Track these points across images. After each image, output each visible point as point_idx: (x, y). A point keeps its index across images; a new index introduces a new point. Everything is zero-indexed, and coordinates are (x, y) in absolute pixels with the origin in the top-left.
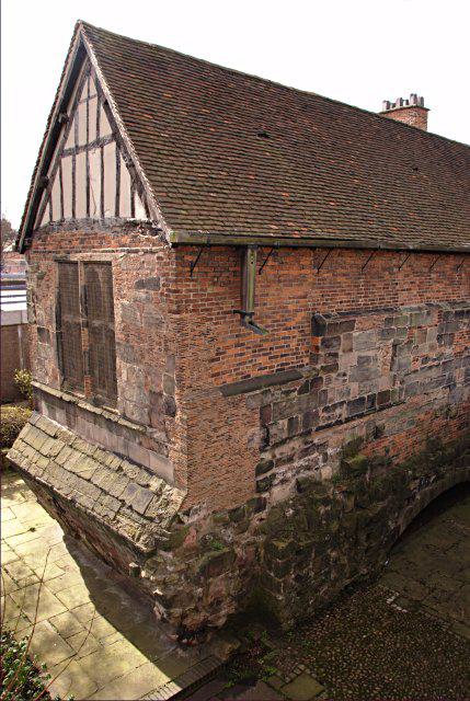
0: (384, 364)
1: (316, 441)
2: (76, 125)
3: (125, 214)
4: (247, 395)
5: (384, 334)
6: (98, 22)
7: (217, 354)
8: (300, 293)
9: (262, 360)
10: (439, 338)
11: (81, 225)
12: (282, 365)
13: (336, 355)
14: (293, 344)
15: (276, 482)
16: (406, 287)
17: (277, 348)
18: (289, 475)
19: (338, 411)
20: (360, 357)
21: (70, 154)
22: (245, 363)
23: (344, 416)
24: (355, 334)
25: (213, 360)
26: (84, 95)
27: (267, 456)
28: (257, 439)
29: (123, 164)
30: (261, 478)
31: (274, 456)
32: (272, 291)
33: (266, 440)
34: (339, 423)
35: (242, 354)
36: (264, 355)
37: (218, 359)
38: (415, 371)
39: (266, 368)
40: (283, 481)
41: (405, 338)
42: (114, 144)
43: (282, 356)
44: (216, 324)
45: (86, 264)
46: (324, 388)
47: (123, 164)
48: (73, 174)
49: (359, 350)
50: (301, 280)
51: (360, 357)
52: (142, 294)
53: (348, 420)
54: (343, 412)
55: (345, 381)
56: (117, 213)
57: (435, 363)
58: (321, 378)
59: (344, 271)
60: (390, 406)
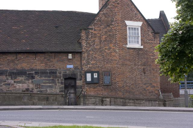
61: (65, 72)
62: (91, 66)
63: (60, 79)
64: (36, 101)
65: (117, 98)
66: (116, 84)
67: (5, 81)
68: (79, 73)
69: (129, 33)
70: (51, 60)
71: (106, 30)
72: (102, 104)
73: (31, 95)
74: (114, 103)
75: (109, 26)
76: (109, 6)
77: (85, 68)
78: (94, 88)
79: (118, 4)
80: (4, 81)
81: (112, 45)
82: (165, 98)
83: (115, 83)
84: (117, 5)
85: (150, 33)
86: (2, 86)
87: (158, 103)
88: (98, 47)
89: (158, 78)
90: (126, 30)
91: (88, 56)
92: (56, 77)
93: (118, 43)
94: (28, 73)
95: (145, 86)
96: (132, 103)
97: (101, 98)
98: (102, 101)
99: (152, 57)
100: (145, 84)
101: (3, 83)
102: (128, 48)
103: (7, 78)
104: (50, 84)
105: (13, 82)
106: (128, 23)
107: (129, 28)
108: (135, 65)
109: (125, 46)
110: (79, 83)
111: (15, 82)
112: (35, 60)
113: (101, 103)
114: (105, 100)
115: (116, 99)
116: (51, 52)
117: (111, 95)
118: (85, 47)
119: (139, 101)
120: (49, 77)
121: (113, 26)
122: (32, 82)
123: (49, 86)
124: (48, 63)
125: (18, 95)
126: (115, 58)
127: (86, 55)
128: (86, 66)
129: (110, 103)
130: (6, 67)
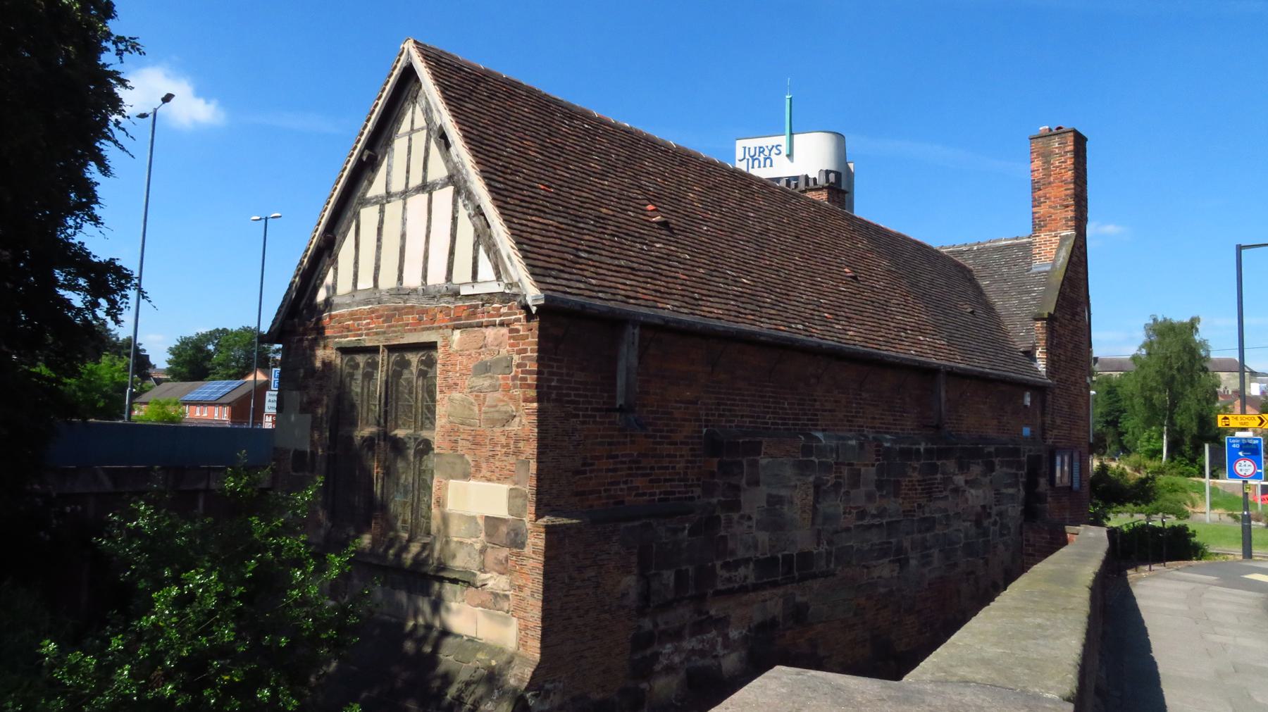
0: (804, 512)
1: (713, 612)
2: (389, 166)
3: (462, 273)
4: (623, 525)
5: (803, 467)
7: (584, 465)
9: (638, 482)
10: (880, 485)
11: (385, 298)
12: (665, 493)
13: (737, 488)
14: (680, 466)
15: (658, 667)
17: (659, 468)
18: (677, 659)
19: (742, 571)
20: (770, 496)
21: (376, 203)
22: (618, 483)
23: (752, 580)
25: (577, 472)
26: (405, 126)
27: (647, 624)
28: (633, 595)
29: (463, 214)
30: (638, 656)
31: (656, 625)
33: (645, 597)
34: (744, 589)
35: (615, 470)
36: (644, 475)
37: (584, 472)
38: (848, 530)
39: (644, 494)
40: (669, 669)
41: (830, 478)
42: (450, 190)
43: (666, 480)
44: (583, 423)
45: (392, 349)
46: (723, 533)
47: (463, 214)
48: (380, 230)
51: (770, 496)
52: (484, 382)
53: (756, 588)
54: (747, 573)
55: (750, 527)
56: (449, 277)
57: (876, 521)
58: (718, 517)
60: (814, 576)
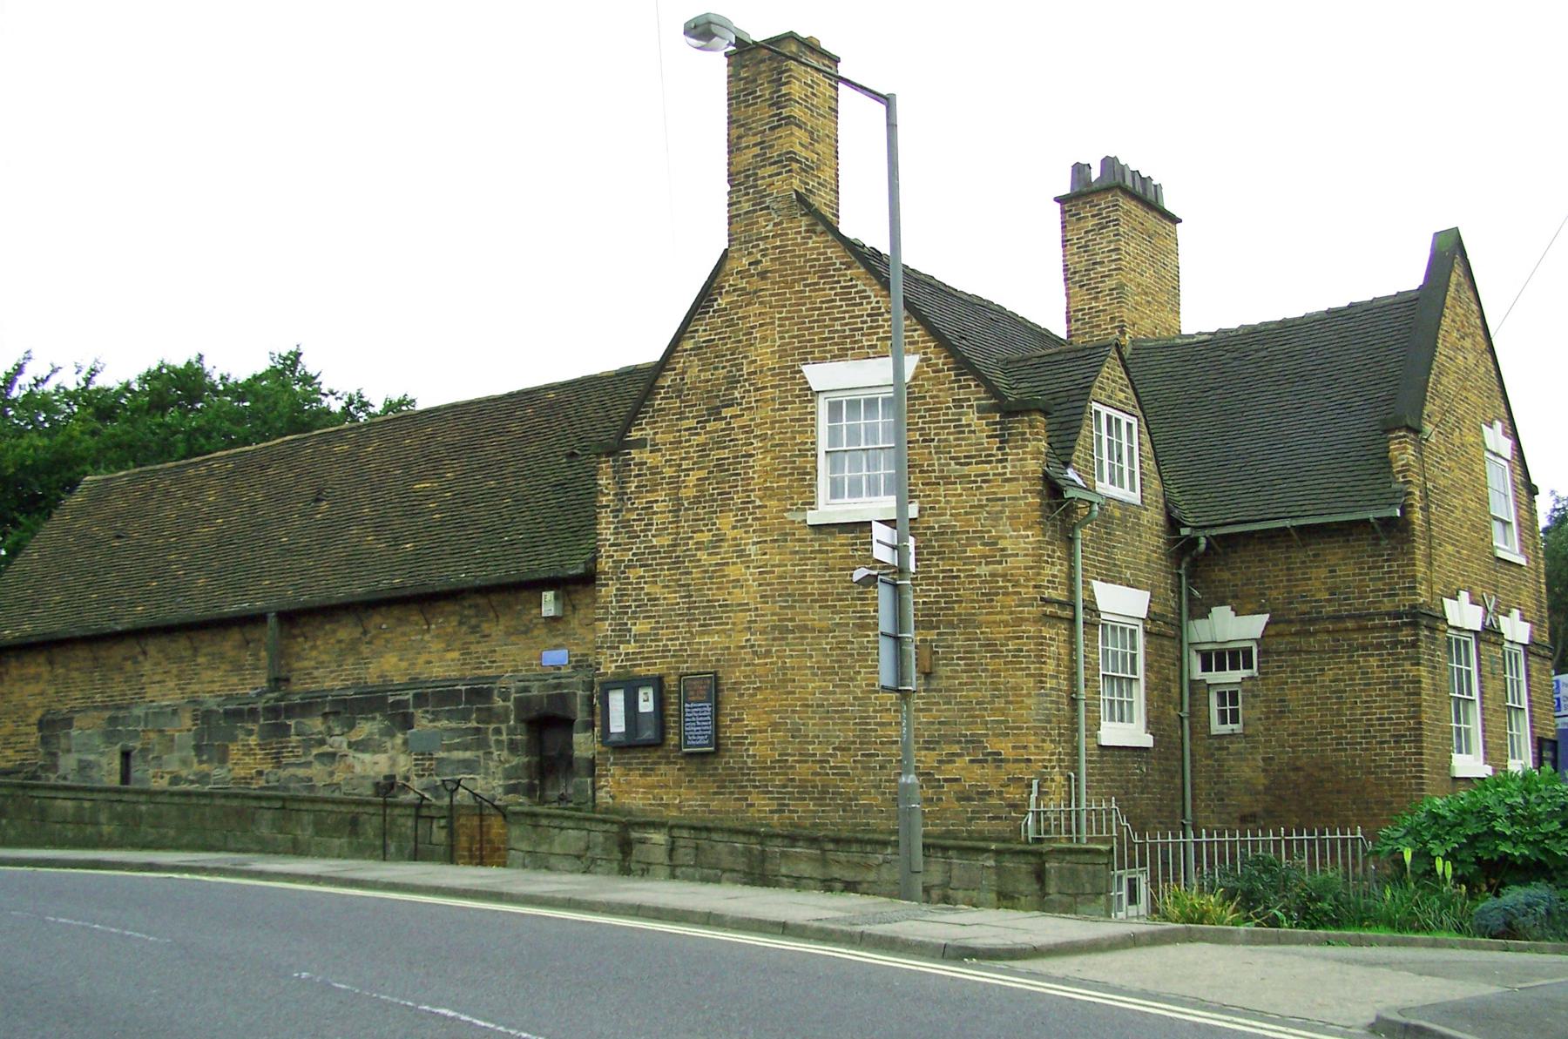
6: (1164, 191)
8: (36, 691)
9: (9, 753)
16: (157, 678)
20: (80, 761)
24: (74, 732)
32: (16, 689)
49: (79, 751)
50: (37, 678)
59: (77, 665)
61: (526, 689)
62: (632, 648)
63: (503, 727)
64: (305, 834)
65: (708, 829)
66: (743, 744)
67: (322, 742)
68: (580, 693)
69: (834, 434)
70: (485, 626)
71: (702, 439)
72: (624, 860)
73: (283, 808)
74: (696, 856)
75: (715, 413)
76: (722, 302)
77: (609, 668)
78: (647, 771)
79: (763, 275)
80: (317, 741)
81: (726, 522)
82: (1046, 832)
83: (739, 742)
84: (757, 283)
85: (971, 418)
86: (311, 763)
87: (991, 863)
88: (666, 540)
89: (1028, 701)
90: (806, 422)
91: (621, 594)
92: (489, 715)
93: (758, 503)
94: (391, 700)
95: (929, 758)
96: (810, 859)
97: (615, 828)
98: (626, 846)
99: (983, 570)
100: (930, 745)
101: (315, 752)
102: (818, 528)
103: (329, 728)
104: (468, 755)
105: (345, 745)
106: (819, 375)
107: (835, 408)
108: (862, 627)
109: (799, 517)
110: (583, 744)
111: (350, 745)
112: (427, 637)
113: (620, 856)
114: (643, 841)
115: (704, 835)
116: (485, 590)
117: (720, 812)
118: (611, 545)
119: (854, 847)
120: (465, 717)
121: (736, 410)
122: (405, 742)
123: (464, 761)
124: (473, 648)
125: (235, 803)
126: (740, 595)
127: (612, 589)
128: (614, 652)
129: (671, 857)
130: (333, 675)
